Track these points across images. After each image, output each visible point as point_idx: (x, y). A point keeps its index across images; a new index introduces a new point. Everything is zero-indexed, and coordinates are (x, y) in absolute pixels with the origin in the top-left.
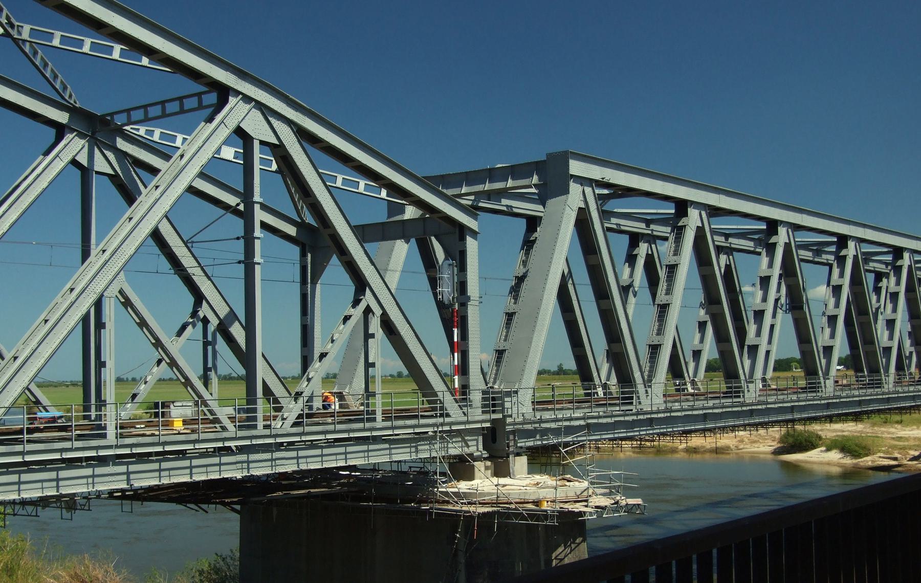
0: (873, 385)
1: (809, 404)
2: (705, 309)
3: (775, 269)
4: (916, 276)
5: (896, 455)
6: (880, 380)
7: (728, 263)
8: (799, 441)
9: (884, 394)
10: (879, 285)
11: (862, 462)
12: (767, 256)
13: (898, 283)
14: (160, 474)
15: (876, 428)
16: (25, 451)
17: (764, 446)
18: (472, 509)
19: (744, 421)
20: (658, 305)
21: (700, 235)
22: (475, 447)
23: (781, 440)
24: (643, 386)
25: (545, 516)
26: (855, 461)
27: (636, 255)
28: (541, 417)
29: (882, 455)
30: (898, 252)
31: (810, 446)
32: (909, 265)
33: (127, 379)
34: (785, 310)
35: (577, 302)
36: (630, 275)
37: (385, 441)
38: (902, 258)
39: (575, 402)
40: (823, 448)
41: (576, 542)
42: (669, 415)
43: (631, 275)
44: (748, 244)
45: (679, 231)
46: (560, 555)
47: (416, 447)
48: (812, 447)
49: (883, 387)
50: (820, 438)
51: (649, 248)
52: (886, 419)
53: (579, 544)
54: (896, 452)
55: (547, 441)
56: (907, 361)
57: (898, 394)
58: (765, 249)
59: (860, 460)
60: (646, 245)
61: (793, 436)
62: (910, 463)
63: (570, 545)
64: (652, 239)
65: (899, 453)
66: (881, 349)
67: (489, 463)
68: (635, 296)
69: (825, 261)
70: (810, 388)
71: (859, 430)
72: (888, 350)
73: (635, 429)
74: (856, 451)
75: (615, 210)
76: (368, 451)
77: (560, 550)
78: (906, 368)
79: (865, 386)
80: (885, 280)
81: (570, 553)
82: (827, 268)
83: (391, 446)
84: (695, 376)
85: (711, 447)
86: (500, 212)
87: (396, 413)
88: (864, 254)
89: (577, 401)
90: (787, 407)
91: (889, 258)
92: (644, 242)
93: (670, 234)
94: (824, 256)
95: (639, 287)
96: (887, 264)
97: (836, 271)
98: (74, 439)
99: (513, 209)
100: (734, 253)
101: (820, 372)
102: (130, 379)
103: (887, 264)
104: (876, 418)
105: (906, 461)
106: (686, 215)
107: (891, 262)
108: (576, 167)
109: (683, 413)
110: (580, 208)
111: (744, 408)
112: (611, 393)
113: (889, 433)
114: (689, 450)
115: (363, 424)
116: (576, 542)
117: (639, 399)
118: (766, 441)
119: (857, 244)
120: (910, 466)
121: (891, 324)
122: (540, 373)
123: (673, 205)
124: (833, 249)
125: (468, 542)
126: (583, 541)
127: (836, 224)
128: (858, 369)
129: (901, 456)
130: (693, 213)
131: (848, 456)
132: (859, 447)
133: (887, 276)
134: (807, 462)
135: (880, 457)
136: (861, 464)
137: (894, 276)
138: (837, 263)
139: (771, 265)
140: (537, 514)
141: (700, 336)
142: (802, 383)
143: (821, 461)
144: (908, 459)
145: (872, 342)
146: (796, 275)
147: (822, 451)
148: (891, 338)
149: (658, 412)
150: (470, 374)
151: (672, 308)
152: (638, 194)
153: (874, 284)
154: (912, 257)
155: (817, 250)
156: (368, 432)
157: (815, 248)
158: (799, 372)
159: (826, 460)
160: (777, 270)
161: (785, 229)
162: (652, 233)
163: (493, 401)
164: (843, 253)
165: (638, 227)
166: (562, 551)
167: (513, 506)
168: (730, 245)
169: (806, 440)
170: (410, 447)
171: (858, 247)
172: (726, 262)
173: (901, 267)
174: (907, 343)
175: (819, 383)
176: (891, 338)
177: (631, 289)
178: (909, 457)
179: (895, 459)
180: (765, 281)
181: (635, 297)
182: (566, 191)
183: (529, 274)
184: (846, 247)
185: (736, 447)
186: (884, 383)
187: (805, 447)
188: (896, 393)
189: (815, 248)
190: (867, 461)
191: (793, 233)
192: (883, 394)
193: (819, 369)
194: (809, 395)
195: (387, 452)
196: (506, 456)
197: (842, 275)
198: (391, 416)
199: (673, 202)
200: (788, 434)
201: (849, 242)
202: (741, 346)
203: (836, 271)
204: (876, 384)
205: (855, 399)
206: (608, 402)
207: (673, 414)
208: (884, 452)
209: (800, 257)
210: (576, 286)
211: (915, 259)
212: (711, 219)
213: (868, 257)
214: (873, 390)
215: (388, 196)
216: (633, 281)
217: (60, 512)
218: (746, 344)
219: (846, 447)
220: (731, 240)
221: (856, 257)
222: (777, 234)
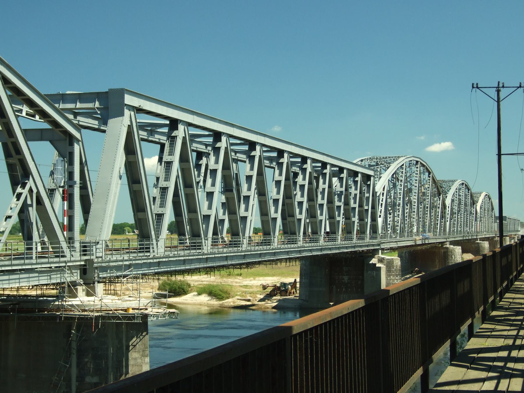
0: (144, 249)
3: (220, 165)
4: (264, 164)
5: (249, 298)
6: (201, 243)
7: (207, 163)
8: (174, 288)
9: (204, 255)
10: (296, 181)
11: (225, 303)
14: (19, 281)
15: (224, 279)
16: (12, 264)
17: (145, 292)
18: (91, 314)
20: (161, 188)
22: (76, 277)
25: (133, 317)
26: (221, 302)
28: (124, 258)
29: (239, 298)
30: (217, 136)
31: (182, 292)
34: (221, 192)
37: (37, 272)
38: (220, 141)
39: (114, 250)
41: (143, 335)
46: (135, 343)
47: (50, 276)
48: (184, 293)
49: (203, 249)
50: (189, 286)
52: (230, 273)
53: (144, 336)
55: (113, 274)
56: (220, 227)
59: (224, 301)
61: (169, 285)
62: (260, 303)
63: (140, 337)
65: (250, 296)
66: (202, 216)
67: (84, 287)
69: (157, 140)
70: (192, 246)
71: (212, 280)
72: (207, 218)
73: (151, 268)
74: (220, 295)
76: (29, 278)
77: (134, 339)
78: (187, 234)
79: (189, 248)
80: (204, 159)
81: (140, 341)
83: (40, 275)
87: (51, 254)
89: (114, 249)
90: (181, 260)
91: (246, 148)
93: (166, 141)
94: (157, 136)
96: (207, 145)
99: (161, 140)
103: (207, 145)
104: (224, 272)
105: (256, 302)
107: (211, 143)
108: (129, 100)
112: (225, 242)
113: (236, 282)
116: (143, 335)
118: (146, 289)
119: (227, 138)
120: (261, 305)
121: (210, 195)
124: (165, 130)
125: (80, 335)
126: (147, 334)
128: (181, 234)
129: (252, 298)
131: (214, 298)
132: (222, 292)
133: (208, 155)
135: (238, 299)
136: (226, 304)
138: (277, 167)
140: (128, 316)
142: (135, 244)
144: (258, 300)
145: (195, 211)
147: (194, 295)
148: (210, 207)
150: (75, 231)
152: (162, 117)
154: (228, 141)
155: (152, 129)
156: (10, 267)
157: (149, 129)
158: (132, 236)
159: (198, 302)
163: (85, 249)
166: (135, 341)
167: (111, 312)
168: (79, 123)
169: (179, 288)
170: (48, 276)
171: (186, 129)
174: (221, 211)
176: (210, 207)
178: (258, 299)
179: (249, 300)
182: (122, 114)
183: (297, 194)
184: (220, 140)
186: (204, 246)
187: (179, 292)
189: (149, 129)
190: (230, 302)
193: (186, 232)
195: (37, 278)
196: (92, 283)
197: (217, 162)
198: (11, 258)
203: (277, 172)
205: (180, 258)
208: (240, 295)
210: (90, 172)
211: (230, 142)
214: (232, 249)
215: (40, 118)
216: (297, 193)
221: (184, 138)
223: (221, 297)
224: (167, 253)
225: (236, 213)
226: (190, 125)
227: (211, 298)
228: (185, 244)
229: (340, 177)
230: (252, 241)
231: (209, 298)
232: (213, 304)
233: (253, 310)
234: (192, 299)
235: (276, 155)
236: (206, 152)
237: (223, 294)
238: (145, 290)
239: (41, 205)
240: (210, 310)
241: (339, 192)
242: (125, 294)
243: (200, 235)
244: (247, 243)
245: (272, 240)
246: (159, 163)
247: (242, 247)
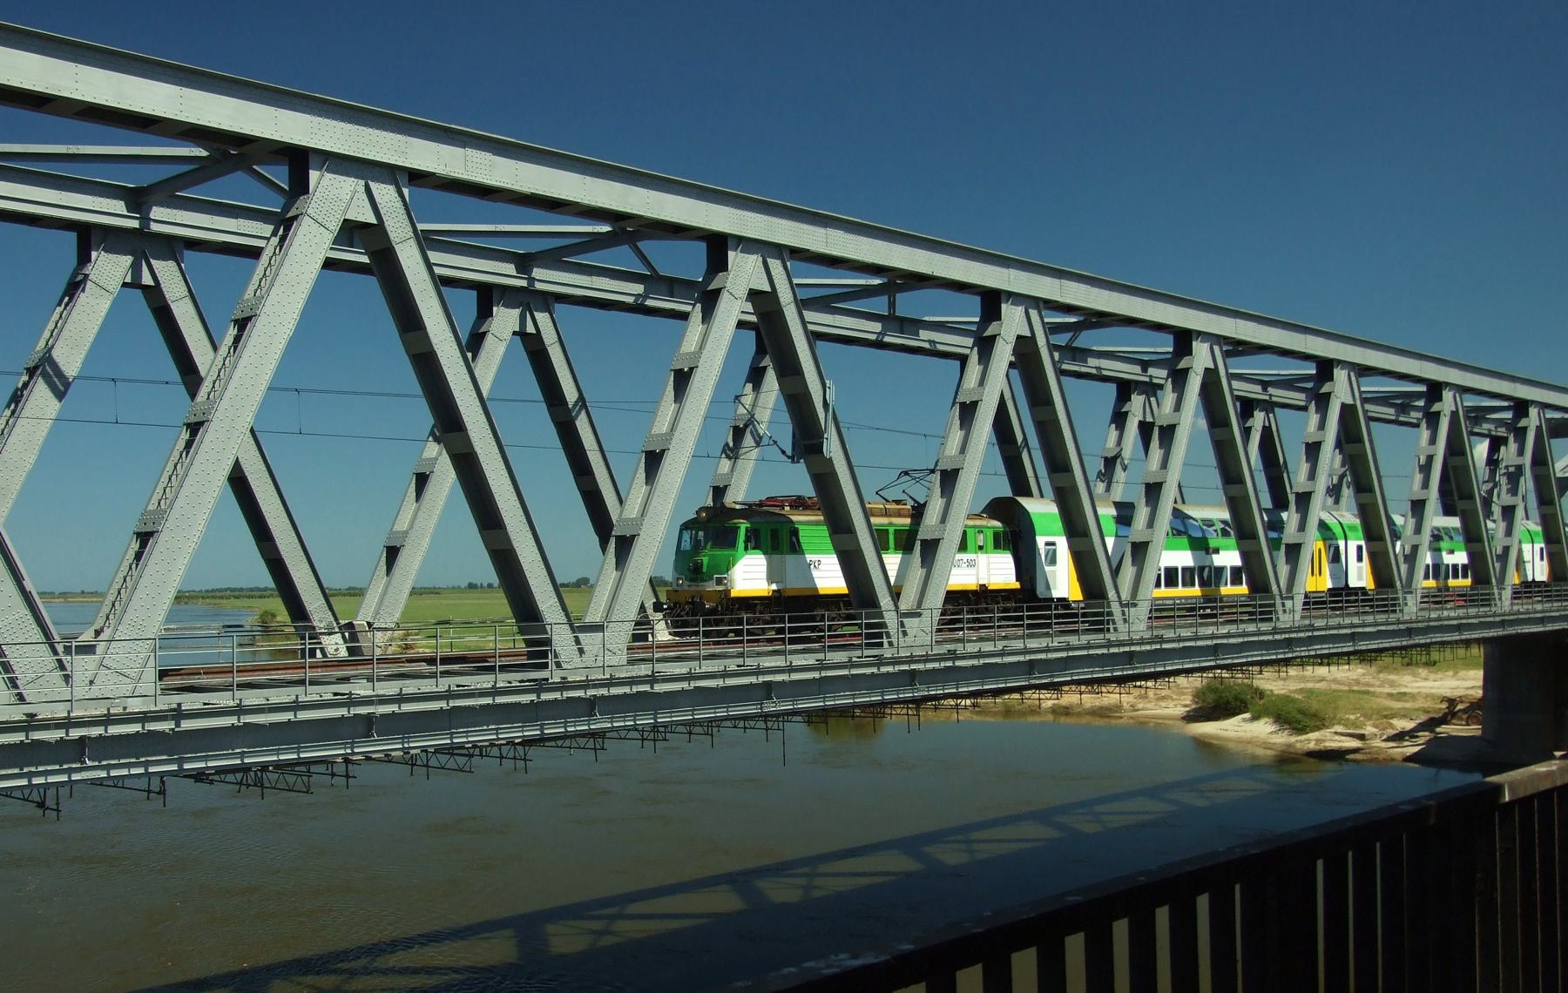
2: (1333, 498)
5: (1369, 730)
12: (1427, 429)
13: (1521, 452)
21: (1211, 381)
23: (1199, 695)
26: (1293, 739)
27: (1127, 413)
29: (1340, 729)
32: (1452, 412)
33: (482, 585)
35: (599, 454)
38: (1440, 399)
39: (657, 647)
40: (1247, 715)
42: (950, 664)
44: (1298, 398)
45: (1179, 378)
54: (1368, 723)
57: (1161, 643)
58: (1170, 379)
60: (1262, 414)
68: (1125, 470)
69: (1094, 371)
75: (926, 319)
85: (1092, 707)
86: (613, 305)
88: (1468, 410)
91: (1508, 415)
92: (1138, 394)
99: (937, 345)
100: (1277, 410)
101: (1494, 580)
102: (485, 585)
106: (1189, 352)
107: (1169, 356)
110: (1019, 338)
114: (1057, 711)
117: (16, 686)
122: (180, 598)
123: (1314, 365)
124: (1421, 403)
127: (1105, 293)
130: (1201, 351)
131: (1286, 729)
133: (1504, 441)
134: (1218, 738)
135: (1336, 733)
137: (1515, 442)
139: (1322, 426)
143: (1240, 738)
144: (1385, 737)
146: (1360, 440)
149: (1142, 642)
151: (962, 476)
153: (1114, 407)
154: (1542, 415)
155: (1402, 403)
160: (1527, 459)
161: (1206, 346)
162: (1271, 398)
164: (1436, 407)
168: (1271, 398)
171: (1458, 399)
172: (1264, 422)
173: (1525, 429)
177: (1119, 460)
179: (1362, 737)
180: (1313, 450)
181: (60, 401)
184: (1526, 415)
185: (1131, 706)
186: (1281, 612)
187: (1235, 709)
188: (1158, 642)
189: (1399, 402)
191: (1356, 379)
192: (1275, 631)
194: (1481, 609)
199: (1170, 333)
200: (1209, 689)
201: (1336, 372)
202: (1274, 545)
204: (1482, 600)
206: (1239, 611)
207: (958, 663)
209: (1236, 393)
212: (1361, 379)
213: (1477, 415)
216: (1122, 449)
217: (334, 770)
218: (918, 537)
219: (1291, 716)
220: (1271, 390)
221: (1454, 414)
222: (1190, 353)
224: (1515, 608)
226: (1465, 390)
229: (1516, 428)
232: (1274, 744)
233: (1355, 761)
234: (1236, 729)
235: (1314, 372)
236: (1144, 383)
240: (1276, 756)
241: (1512, 469)
244: (934, 629)
245: (1493, 594)
246: (1337, 451)
247: (1401, 611)
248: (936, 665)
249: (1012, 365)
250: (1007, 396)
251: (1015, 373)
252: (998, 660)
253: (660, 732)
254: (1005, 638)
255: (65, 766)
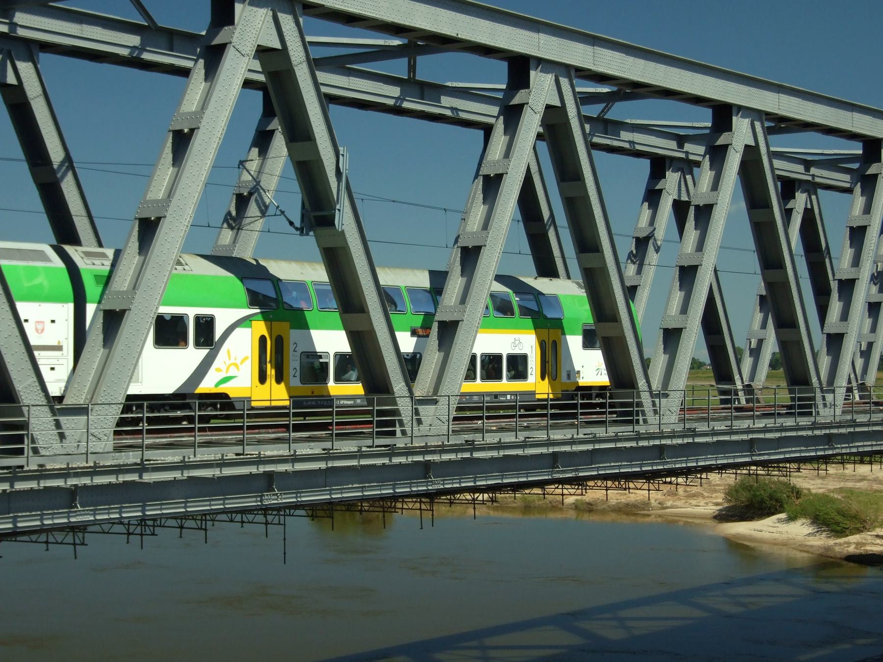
1: (718, 441)
2: (878, 286)
6: (813, 399)
7: (809, 206)
12: (862, 195)
19: (68, 517)
24: (648, 394)
26: (831, 542)
27: (661, 191)
35: (86, 220)
36: (650, 223)
40: (783, 516)
42: (690, 440)
43: (652, 222)
44: (842, 179)
45: (718, 154)
51: (682, 180)
64: (811, 187)
74: (838, 524)
82: (481, 133)
84: (752, 378)
92: (802, 192)
95: (664, 241)
97: (499, 139)
98: (196, 446)
100: (819, 191)
106: (729, 128)
107: (707, 131)
109: (715, 439)
110: (747, 146)
111: (817, 432)
115: (242, 447)
123: (861, 144)
131: (824, 531)
133: (687, 166)
136: (837, 549)
141: (871, 322)
149: (673, 435)
161: (746, 122)
165: (665, 147)
168: (813, 179)
175: (640, 404)
177: (651, 242)
186: (821, 406)
190: (849, 544)
200: (743, 486)
212: (770, 137)
216: (655, 229)
220: (813, 170)
223: (840, 528)
225: (795, 325)
227: (816, 530)
228: (734, 403)
230: (758, 401)
231: (811, 528)
234: (771, 529)
235: (861, 152)
237: (846, 522)
238: (711, 497)
239: (617, 322)
242: (665, 505)
243: (807, 380)
248: (452, 456)
249: (539, 137)
250: (534, 169)
251: (543, 146)
252: (519, 452)
253: (149, 526)
254: (527, 428)
255: (809, 448)
